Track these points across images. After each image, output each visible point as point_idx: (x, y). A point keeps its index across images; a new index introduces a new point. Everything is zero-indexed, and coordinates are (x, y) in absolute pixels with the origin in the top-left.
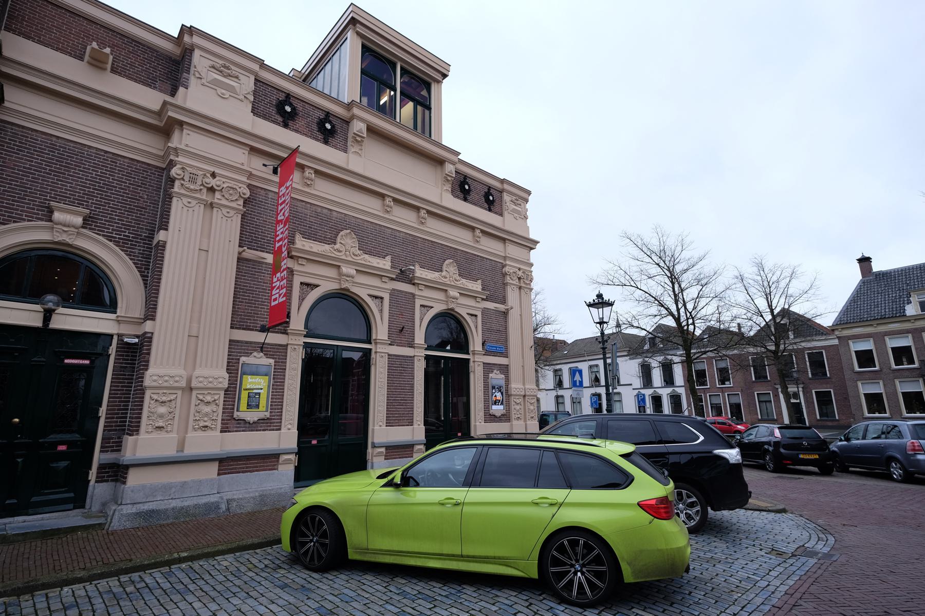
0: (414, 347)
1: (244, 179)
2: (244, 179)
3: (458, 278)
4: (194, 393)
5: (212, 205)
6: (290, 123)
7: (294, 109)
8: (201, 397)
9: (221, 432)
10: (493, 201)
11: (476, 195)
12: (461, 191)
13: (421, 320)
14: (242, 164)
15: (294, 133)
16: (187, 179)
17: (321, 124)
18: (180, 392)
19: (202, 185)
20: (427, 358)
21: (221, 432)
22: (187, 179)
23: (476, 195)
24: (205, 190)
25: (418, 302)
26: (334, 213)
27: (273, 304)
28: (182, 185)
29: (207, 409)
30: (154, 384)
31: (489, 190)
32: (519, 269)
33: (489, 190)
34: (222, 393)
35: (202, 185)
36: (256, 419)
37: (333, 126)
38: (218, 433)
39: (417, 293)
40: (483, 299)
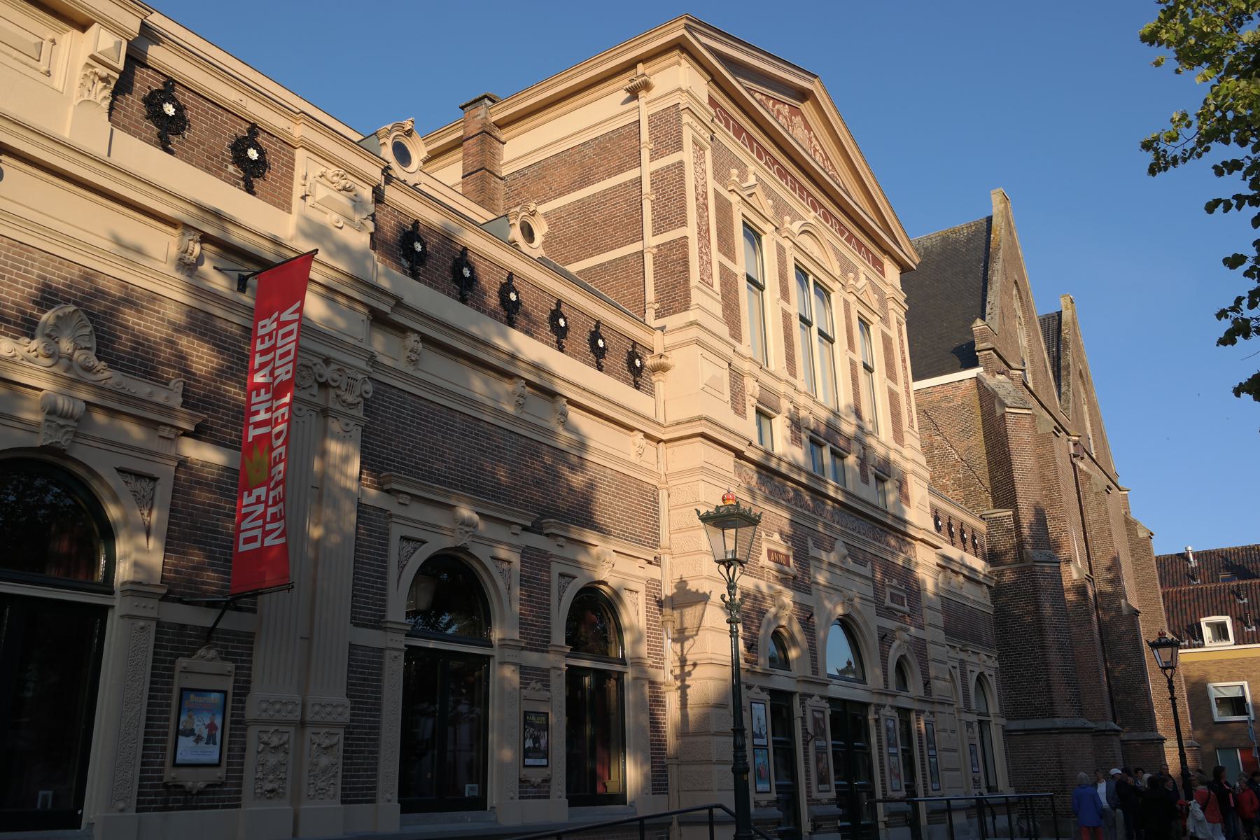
0: (385, 629)
1: (362, 364)
2: (362, 364)
3: (93, 361)
4: (309, 731)
5: (325, 413)
6: (175, 139)
7: (180, 108)
8: (265, 737)
9: (138, 810)
10: (566, 328)
11: (578, 337)
12: (630, 371)
13: (402, 568)
14: (361, 341)
15: (471, 310)
16: (343, 387)
17: (238, 149)
18: (292, 729)
19: (361, 395)
20: (411, 652)
21: (138, 810)
22: (343, 387)
23: (615, 359)
24: (316, 386)
25: (396, 531)
26: (609, 471)
27: (243, 548)
28: (338, 396)
29: (272, 760)
30: (317, 718)
31: (597, 327)
32: (327, 361)
33: (597, 327)
34: (342, 732)
35: (361, 395)
36: (201, 785)
37: (180, 108)
38: (336, 804)
39: (554, 550)
40: (525, 529)
